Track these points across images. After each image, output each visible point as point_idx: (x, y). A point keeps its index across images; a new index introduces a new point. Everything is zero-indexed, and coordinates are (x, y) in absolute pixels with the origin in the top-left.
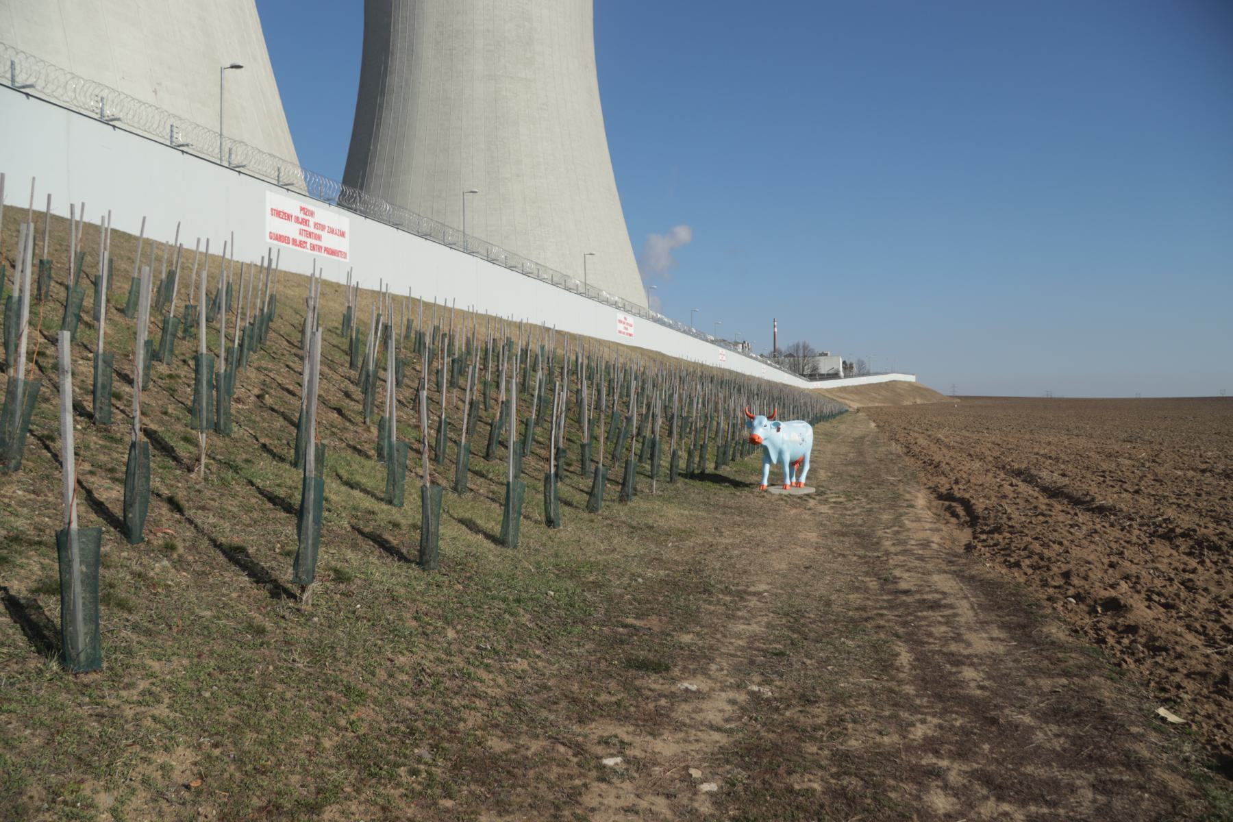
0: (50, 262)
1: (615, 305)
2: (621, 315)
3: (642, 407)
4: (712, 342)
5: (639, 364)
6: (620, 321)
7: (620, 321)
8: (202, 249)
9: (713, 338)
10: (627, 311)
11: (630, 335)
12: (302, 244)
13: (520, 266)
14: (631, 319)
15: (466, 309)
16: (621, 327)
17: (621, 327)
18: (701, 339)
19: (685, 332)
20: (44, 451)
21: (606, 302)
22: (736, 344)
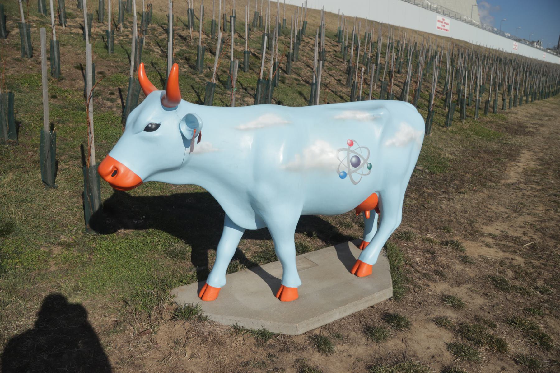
0: (286, 20)
1: (437, 11)
2: (440, 17)
3: (381, 73)
4: (509, 38)
5: (361, 32)
6: (439, 21)
7: (439, 21)
8: (304, 6)
9: (509, 35)
10: (445, 15)
11: (447, 30)
12: (441, 29)
13: (421, 3)
14: (447, 20)
15: (301, 6)
16: (439, 25)
17: (439, 25)
18: (500, 35)
19: (489, 30)
20: (197, 91)
21: (427, 7)
22: (533, 42)
